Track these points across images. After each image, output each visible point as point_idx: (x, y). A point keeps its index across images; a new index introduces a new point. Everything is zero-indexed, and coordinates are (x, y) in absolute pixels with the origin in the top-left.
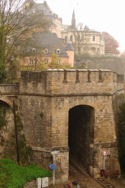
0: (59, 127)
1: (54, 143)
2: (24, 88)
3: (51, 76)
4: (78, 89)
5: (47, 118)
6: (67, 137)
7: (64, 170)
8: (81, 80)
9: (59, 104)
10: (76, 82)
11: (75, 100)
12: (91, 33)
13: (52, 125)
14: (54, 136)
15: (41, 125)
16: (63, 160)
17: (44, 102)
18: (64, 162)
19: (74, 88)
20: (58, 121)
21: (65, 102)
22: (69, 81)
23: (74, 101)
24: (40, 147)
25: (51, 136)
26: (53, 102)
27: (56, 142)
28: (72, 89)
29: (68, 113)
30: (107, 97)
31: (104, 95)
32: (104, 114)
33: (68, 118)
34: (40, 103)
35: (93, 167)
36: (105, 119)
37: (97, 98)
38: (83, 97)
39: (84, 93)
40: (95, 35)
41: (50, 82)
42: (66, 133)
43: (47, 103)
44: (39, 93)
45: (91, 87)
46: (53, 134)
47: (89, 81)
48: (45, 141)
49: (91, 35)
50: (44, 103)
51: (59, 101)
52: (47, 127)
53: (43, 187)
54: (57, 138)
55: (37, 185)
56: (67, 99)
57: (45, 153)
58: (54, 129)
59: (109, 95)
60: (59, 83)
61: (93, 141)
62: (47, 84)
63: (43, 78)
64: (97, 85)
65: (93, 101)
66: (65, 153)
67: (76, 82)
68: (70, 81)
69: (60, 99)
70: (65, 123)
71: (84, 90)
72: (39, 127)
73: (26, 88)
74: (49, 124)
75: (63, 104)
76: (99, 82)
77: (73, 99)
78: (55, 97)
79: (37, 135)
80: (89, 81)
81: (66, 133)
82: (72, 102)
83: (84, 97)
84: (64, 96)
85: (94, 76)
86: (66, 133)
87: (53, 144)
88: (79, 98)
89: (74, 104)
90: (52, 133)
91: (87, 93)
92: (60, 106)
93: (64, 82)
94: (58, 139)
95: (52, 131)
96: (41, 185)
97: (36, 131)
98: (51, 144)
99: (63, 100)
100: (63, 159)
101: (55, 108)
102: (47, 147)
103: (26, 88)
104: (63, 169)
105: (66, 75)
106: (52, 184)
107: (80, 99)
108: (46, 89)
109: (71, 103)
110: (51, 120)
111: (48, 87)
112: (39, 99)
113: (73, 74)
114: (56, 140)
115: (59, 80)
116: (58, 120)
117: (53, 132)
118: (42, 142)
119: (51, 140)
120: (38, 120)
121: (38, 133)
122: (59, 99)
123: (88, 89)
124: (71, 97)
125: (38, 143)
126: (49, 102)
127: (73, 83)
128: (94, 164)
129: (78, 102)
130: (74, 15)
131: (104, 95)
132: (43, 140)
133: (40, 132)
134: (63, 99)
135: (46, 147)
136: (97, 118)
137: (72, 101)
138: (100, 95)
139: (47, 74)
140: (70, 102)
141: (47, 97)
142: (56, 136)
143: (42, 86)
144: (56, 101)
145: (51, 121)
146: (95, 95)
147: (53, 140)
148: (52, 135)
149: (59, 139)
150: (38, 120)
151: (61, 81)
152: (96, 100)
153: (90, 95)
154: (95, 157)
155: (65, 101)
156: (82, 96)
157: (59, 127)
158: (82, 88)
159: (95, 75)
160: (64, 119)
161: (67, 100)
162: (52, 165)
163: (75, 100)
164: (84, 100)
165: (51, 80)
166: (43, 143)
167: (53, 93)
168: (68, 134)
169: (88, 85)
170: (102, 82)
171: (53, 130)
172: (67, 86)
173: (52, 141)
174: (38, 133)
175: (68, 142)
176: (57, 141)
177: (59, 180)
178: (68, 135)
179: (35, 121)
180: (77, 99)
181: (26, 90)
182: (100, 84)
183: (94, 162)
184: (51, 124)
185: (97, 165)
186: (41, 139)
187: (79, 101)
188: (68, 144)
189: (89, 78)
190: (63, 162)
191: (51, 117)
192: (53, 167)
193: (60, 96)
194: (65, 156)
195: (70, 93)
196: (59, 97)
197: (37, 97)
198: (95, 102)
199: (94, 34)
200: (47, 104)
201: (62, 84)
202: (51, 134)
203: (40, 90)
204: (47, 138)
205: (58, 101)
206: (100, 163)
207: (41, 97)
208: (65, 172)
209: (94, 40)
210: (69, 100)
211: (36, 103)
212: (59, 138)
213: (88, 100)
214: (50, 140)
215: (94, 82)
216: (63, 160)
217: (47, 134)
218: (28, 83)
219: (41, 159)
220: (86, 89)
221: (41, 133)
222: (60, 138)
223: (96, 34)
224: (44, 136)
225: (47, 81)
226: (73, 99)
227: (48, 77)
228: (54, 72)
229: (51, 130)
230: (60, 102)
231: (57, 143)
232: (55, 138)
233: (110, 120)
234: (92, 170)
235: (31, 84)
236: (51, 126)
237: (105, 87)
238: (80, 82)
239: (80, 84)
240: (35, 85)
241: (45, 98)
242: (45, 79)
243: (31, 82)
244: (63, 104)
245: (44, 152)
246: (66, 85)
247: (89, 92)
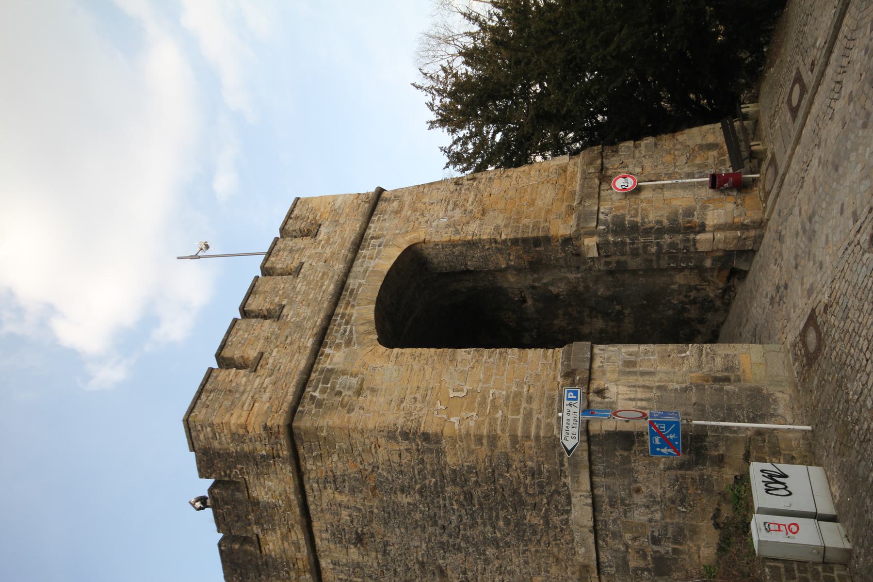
0: (451, 391)
1: (535, 420)
3: (209, 429)
5: (400, 455)
6: (513, 353)
7: (706, 370)
9: (339, 393)
13: (430, 431)
14: (496, 419)
15: (445, 500)
16: (643, 374)
17: (330, 473)
18: (652, 369)
19: (299, 326)
20: (419, 398)
23: (349, 327)
24: (568, 512)
25: (493, 439)
26: (322, 422)
27: (528, 415)
29: (396, 350)
33: (419, 350)
35: (702, 228)
36: (473, 202)
38: (347, 291)
39: (332, 287)
41: (236, 437)
42: (489, 357)
43: (330, 455)
44: (292, 497)
45: (322, 263)
46: (478, 426)
48: (526, 478)
50: (332, 471)
51: (323, 391)
52: (446, 464)
53: (826, 507)
54: (506, 405)
55: (819, 559)
57: (596, 479)
58: (452, 419)
60: (248, 389)
61: (567, 241)
62: (247, 448)
63: (225, 472)
66: (597, 364)
69: (320, 385)
70: (437, 366)
72: (455, 507)
73: (288, 564)
74: (431, 451)
75: (344, 373)
77: (337, 331)
78: (300, 408)
79: (501, 523)
81: (492, 360)
82: (351, 332)
83: (351, 287)
86: (489, 357)
87: (538, 427)
89: (363, 324)
90: (472, 432)
92: (349, 388)
94: (514, 401)
95: (463, 432)
96: (811, 521)
97: (481, 528)
98: (537, 437)
100: (635, 373)
102: (562, 465)
103: (292, 566)
104: (700, 374)
105: (232, 359)
106: (811, 439)
107: (352, 303)
108: (268, 455)
109: (355, 336)
110: (405, 435)
111: (258, 445)
112: (322, 498)
113: (241, 332)
115: (237, 391)
116: (415, 399)
117: (472, 424)
118: (537, 499)
119: (514, 439)
120: (422, 512)
121: (490, 518)
122: (317, 394)
123: (324, 274)
124: (328, 340)
125: (547, 523)
126: (326, 443)
127: (273, 333)
128: (687, 227)
129: (363, 311)
132: (522, 490)
133: (481, 504)
135: (561, 473)
136: (457, 232)
137: (347, 333)
142: (495, 407)
143: (258, 476)
145: (411, 436)
147: (515, 430)
148: (485, 432)
149: (518, 394)
150: (422, 512)
154: (643, 222)
155: (336, 364)
156: (344, 293)
157: (451, 391)
160: (416, 367)
162: (657, 440)
163: (347, 323)
165: (226, 431)
166: (541, 493)
168: (498, 350)
170: (320, 225)
171: (456, 425)
173: (519, 434)
174: (490, 518)
175: (540, 351)
176: (524, 405)
177: (775, 401)
178: (503, 350)
179: (430, 529)
181: (300, 564)
183: (674, 229)
184: (426, 437)
185: (689, 212)
186: (522, 503)
187: (359, 304)
188: (551, 351)
190: (651, 374)
191: (391, 436)
192: (672, 437)
194: (620, 363)
196: (308, 389)
197: (312, 507)
200: (335, 458)
201: (258, 379)
203: (281, 489)
204: (509, 466)
206: (675, 203)
207: (307, 487)
208: (718, 360)
211: (345, 514)
212: (508, 397)
213: (366, 271)
214: (513, 446)
216: (643, 374)
217: (484, 461)
219: (643, 509)
220: (322, 278)
221: (487, 497)
222: (514, 389)
224: (501, 481)
226: (336, 334)
228: (192, 414)
229: (460, 436)
231: (535, 406)
232: (505, 418)
234: (719, 235)
235: (269, 538)
239: (291, 302)
241: (309, 467)
243: (257, 536)
244: (344, 373)
245: (593, 486)
246: (271, 361)
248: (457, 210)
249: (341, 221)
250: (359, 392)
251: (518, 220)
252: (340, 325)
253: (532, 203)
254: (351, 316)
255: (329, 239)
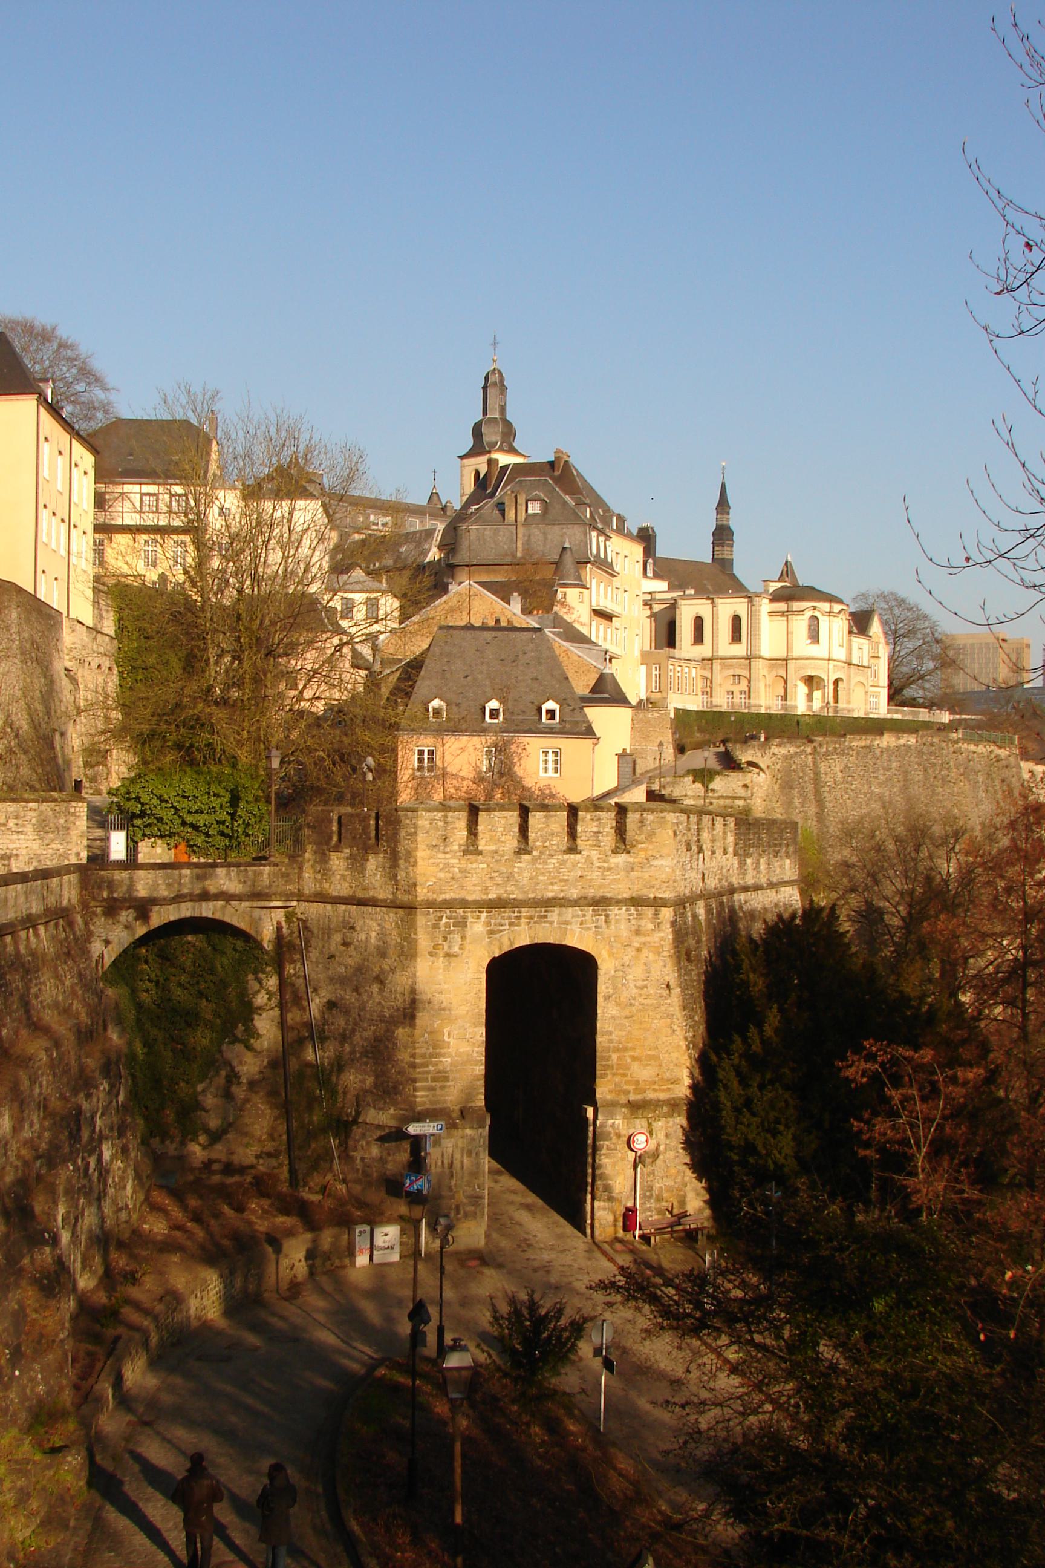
2: (319, 876)
4: (528, 877)
8: (538, 844)
10: (519, 852)
11: (511, 924)
12: (796, 605)
19: (509, 877)
21: (469, 932)
22: (488, 848)
28: (499, 880)
30: (649, 912)
31: (636, 902)
32: (640, 983)
34: (374, 934)
37: (607, 916)
39: (550, 895)
40: (817, 614)
45: (580, 874)
47: (573, 850)
49: (801, 612)
51: (447, 925)
56: (479, 917)
59: (657, 903)
64: (606, 865)
65: (589, 929)
67: (519, 852)
68: (494, 848)
71: (552, 884)
75: (463, 938)
76: (615, 852)
80: (573, 850)
84: (464, 904)
85: (595, 829)
88: (531, 917)
91: (562, 895)
93: (466, 852)
99: (462, 924)
101: (431, 954)
114: (434, 1080)
122: (444, 920)
129: (523, 934)
130: (723, 505)
131: (636, 902)
134: (465, 917)
136: (607, 998)
138: (619, 902)
139: (398, 822)
140: (491, 932)
141: (401, 912)
144: (436, 926)
146: (600, 903)
151: (456, 848)
152: (604, 925)
153: (575, 903)
158: (541, 878)
159: (595, 823)
161: (477, 926)
163: (511, 924)
164: (551, 923)
167: (422, 893)
169: (569, 865)
170: (628, 852)
172: (479, 866)
180: (523, 920)
182: (621, 859)
189: (572, 834)
193: (448, 904)
195: (492, 896)
198: (597, 934)
199: (815, 608)
202: (413, 1056)
205: (443, 928)
209: (814, 636)
210: (488, 924)
215: (595, 854)
218: (333, 856)
220: (561, 881)
223: (825, 606)
225: (401, 849)
227: (403, 834)
230: (450, 932)
232: (428, 1072)
233: (663, 1008)
236: (413, 1025)
237: (639, 874)
238: (535, 853)
239: (535, 860)
240: (357, 864)
242: (394, 839)
244: (463, 938)
246: (474, 866)
247: (574, 893)
248: (635, 991)
249: (634, 874)
250: (448, 955)
251: (617, 1050)
252: (510, 918)
253: (634, 1058)
254: (518, 925)
255: (609, 869)
